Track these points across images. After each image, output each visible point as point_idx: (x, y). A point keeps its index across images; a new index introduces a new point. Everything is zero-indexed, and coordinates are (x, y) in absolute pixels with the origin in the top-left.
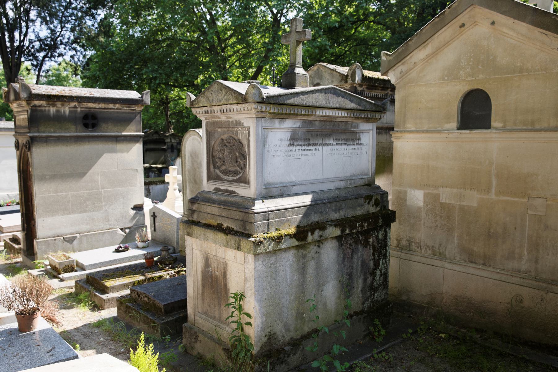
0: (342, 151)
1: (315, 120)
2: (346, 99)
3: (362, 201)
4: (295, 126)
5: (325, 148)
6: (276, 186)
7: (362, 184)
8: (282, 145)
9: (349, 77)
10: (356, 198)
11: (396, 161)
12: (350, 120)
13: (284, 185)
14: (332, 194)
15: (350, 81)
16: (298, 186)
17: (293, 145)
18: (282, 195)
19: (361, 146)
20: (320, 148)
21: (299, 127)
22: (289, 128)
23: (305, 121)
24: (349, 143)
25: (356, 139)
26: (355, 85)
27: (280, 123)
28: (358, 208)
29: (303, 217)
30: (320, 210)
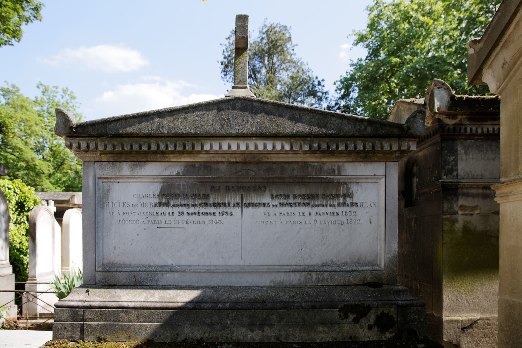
0: (297, 218)
1: (218, 162)
2: (280, 115)
3: (336, 314)
4: (167, 173)
5: (249, 211)
6: (125, 269)
7: (357, 281)
8: (143, 205)
9: (428, 106)
10: (313, 307)
11: (506, 242)
12: (310, 159)
13: (144, 269)
14: (258, 295)
15: (428, 113)
16: (176, 275)
17: (167, 204)
18: (136, 284)
19: (354, 209)
20: (237, 211)
21: (178, 174)
22: (154, 177)
23: (192, 165)
24: (317, 203)
25: (338, 196)
26: (437, 116)
27: (132, 168)
28: (321, 329)
29: (161, 326)
30: (208, 321)
